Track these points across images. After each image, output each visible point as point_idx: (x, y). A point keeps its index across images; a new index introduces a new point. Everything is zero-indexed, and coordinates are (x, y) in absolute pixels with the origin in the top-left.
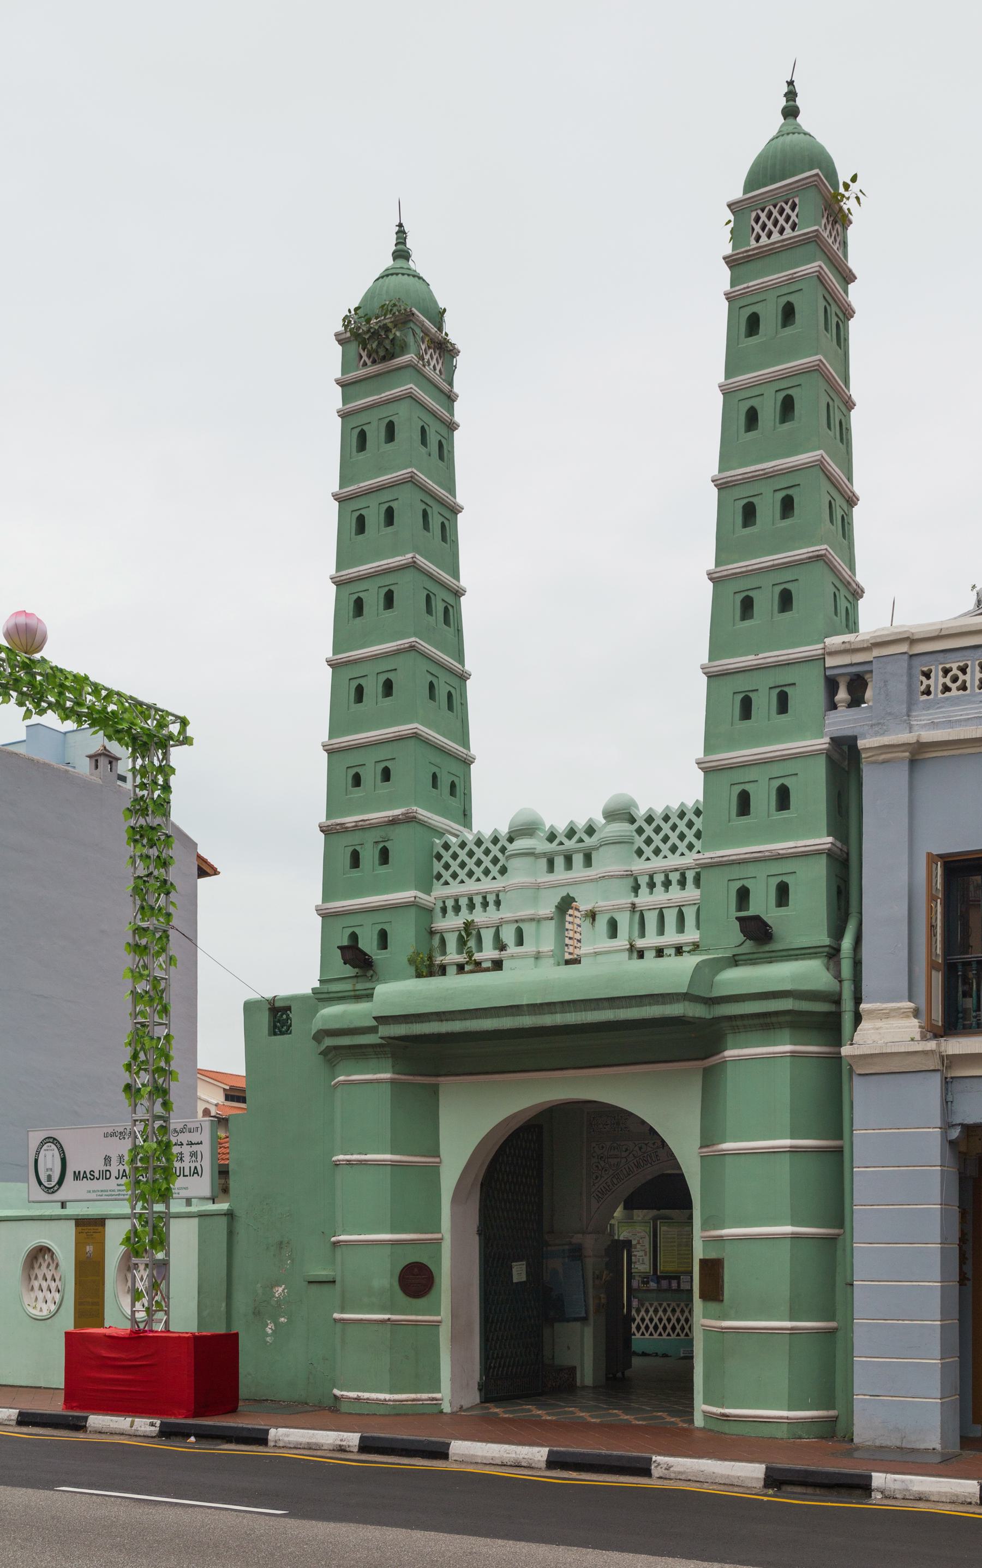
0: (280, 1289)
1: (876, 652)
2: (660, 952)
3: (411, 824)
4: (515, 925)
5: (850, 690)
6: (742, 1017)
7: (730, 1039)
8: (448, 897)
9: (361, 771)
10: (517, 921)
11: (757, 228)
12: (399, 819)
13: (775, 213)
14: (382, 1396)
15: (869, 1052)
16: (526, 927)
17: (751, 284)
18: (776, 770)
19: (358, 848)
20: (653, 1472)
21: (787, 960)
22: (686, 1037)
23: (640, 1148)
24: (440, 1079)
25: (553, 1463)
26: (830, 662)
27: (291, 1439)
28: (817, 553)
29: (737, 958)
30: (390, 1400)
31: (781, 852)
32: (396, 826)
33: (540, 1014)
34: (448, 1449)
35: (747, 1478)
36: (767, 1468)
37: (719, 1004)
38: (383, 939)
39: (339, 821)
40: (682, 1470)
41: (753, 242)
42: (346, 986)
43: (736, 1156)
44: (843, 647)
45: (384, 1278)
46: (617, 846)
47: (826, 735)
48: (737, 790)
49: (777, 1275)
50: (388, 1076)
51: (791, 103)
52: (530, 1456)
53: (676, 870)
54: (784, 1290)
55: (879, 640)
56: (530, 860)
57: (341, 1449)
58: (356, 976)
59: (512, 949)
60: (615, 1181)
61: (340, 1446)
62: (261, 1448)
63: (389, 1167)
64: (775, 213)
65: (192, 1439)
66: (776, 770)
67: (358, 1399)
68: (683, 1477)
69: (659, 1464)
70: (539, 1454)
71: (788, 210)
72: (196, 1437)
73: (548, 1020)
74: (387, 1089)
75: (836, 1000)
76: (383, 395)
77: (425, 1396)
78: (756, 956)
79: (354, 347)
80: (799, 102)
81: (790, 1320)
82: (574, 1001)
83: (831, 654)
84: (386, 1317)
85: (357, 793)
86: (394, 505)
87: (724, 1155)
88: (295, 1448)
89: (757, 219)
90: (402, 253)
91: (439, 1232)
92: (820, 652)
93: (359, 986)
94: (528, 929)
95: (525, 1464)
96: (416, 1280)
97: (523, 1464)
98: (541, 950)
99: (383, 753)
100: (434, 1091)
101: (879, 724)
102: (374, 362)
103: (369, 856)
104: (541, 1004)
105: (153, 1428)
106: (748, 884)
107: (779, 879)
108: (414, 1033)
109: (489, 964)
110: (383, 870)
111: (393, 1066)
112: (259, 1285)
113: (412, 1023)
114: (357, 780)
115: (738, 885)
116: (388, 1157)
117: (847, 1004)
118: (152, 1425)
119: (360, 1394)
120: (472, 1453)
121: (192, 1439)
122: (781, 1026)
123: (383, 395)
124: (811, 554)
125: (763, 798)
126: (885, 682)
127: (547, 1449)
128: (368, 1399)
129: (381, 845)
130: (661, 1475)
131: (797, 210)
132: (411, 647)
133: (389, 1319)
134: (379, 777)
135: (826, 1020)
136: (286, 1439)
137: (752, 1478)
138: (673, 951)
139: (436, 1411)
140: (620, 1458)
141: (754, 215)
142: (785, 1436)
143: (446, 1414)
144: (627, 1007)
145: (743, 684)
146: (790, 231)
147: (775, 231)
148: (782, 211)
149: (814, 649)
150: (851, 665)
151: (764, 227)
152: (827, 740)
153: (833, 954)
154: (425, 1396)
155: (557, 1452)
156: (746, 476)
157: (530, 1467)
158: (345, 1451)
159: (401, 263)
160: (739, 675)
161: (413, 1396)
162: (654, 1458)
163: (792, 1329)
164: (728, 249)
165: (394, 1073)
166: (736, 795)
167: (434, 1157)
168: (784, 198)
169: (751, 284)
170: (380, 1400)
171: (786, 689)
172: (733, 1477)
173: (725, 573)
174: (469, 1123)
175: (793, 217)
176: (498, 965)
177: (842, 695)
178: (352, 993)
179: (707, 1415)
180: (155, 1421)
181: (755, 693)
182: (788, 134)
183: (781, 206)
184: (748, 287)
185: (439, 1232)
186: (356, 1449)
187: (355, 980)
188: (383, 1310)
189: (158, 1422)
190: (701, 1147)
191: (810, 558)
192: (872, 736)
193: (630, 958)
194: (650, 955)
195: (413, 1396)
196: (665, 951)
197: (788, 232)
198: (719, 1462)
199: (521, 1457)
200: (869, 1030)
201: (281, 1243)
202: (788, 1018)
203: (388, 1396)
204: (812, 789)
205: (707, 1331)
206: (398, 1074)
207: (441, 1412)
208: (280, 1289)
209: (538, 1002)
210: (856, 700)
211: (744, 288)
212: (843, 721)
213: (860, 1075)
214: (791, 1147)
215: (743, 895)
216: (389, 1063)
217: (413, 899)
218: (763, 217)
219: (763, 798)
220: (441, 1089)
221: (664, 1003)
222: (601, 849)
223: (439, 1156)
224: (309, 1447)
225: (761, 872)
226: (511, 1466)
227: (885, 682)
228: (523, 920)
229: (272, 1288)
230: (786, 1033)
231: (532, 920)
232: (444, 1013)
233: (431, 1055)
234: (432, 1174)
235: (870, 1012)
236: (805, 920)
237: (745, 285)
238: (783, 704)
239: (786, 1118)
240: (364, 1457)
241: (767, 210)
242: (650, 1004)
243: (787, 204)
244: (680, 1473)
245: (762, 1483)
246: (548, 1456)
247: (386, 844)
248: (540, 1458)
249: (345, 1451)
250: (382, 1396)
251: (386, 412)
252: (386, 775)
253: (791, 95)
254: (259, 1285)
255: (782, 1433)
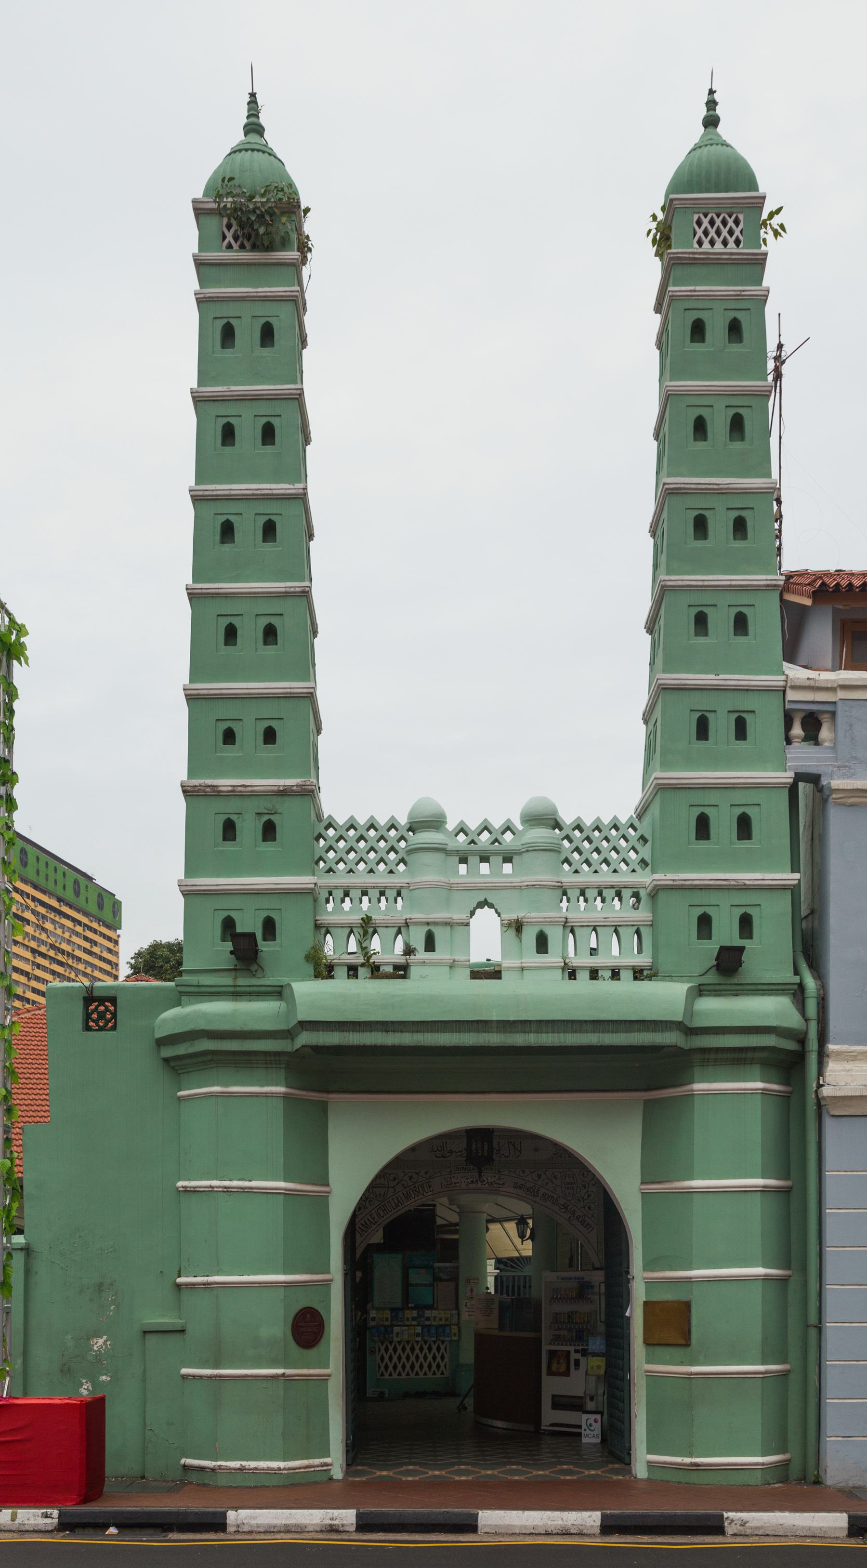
0: (101, 1341)
1: (841, 694)
2: (594, 974)
3: (306, 798)
4: (426, 928)
5: (804, 726)
6: (717, 1050)
7: (697, 1071)
8: (336, 888)
9: (236, 727)
10: (428, 924)
11: (700, 232)
12: (293, 791)
13: (718, 222)
14: (274, 1464)
15: (849, 1094)
16: (438, 932)
17: (698, 288)
18: (739, 797)
19: (234, 818)
20: (726, 1529)
21: (754, 995)
22: (642, 1069)
23: (411, 1178)
24: (331, 1096)
25: (607, 1528)
26: (791, 695)
27: (260, 1521)
28: (774, 583)
29: (702, 988)
30: (285, 1469)
31: (747, 883)
32: (285, 798)
33: (511, 1032)
34: (477, 1520)
35: (830, 1528)
36: (849, 1517)
37: (697, 1034)
38: (269, 927)
39: (209, 782)
40: (759, 1525)
41: (696, 246)
42: (226, 980)
43: (743, 1194)
44: (808, 683)
45: (276, 1327)
46: (548, 853)
47: (790, 769)
48: (697, 812)
49: (752, 1317)
50: (281, 1089)
51: (711, 112)
52: (579, 1522)
53: (612, 887)
54: (755, 1332)
55: (847, 683)
56: (439, 856)
57: (332, 1529)
58: (235, 970)
59: (421, 955)
60: (382, 1213)
61: (331, 1525)
62: (221, 1536)
63: (282, 1197)
64: (718, 222)
65: (113, 1530)
66: (739, 797)
67: (241, 1469)
68: (760, 1532)
69: (732, 1521)
70: (591, 1519)
71: (731, 223)
72: (117, 1526)
73: (519, 1039)
74: (280, 1104)
75: (802, 1040)
76: (260, 290)
77: (317, 1461)
78: (721, 987)
79: (215, 224)
80: (719, 111)
81: (762, 1364)
82: (553, 1022)
83: (793, 687)
84: (280, 1371)
85: (231, 752)
86: (275, 422)
87: (691, 1192)
88: (266, 1532)
89: (699, 223)
90: (254, 128)
91: (329, 1272)
92: (782, 684)
93: (241, 982)
94: (440, 934)
95: (575, 1532)
96: (307, 1328)
97: (572, 1531)
98: (457, 958)
99: (268, 710)
100: (323, 1108)
101: (845, 766)
102: (242, 247)
103: (249, 828)
104: (515, 1022)
105: (48, 1521)
106: (710, 911)
107: (742, 910)
108: (351, 1043)
109: (390, 969)
110: (268, 847)
111: (286, 1079)
112: (69, 1337)
113: (348, 1031)
114: (229, 737)
115: (699, 911)
116: (282, 1184)
117: (813, 1044)
118: (46, 1516)
119: (244, 1463)
120: (507, 1523)
121: (113, 1530)
122: (752, 1062)
123: (260, 290)
124: (769, 582)
125: (723, 825)
126: (851, 725)
127: (599, 1513)
128: (256, 1469)
129: (265, 818)
130: (735, 1531)
131: (741, 226)
132: (303, 592)
133: (283, 1375)
134: (261, 738)
135: (791, 1061)
136: (253, 1522)
137: (836, 1528)
138: (609, 974)
139: (325, 1478)
140: (686, 1517)
141: (696, 217)
142: (759, 1483)
143: (338, 1481)
144: (613, 1032)
145: (703, 703)
146: (734, 246)
147: (706, 242)
148: (724, 223)
149: (775, 680)
150: (813, 702)
151: (706, 233)
152: (792, 775)
153: (798, 993)
154: (317, 1461)
155: (612, 1516)
156: (700, 486)
157: (581, 1534)
158: (337, 1531)
159: (254, 138)
160: (697, 692)
161: (305, 1462)
162: (726, 1515)
163: (766, 1372)
164: (199, 195)
165: (287, 1087)
166: (684, 816)
167: (323, 1185)
168: (729, 210)
169: (698, 288)
170: (273, 1469)
171: (744, 715)
172: (816, 1528)
173: (680, 583)
174: (359, 1152)
175: (737, 232)
176: (401, 971)
177: (797, 730)
178: (231, 989)
179: (650, 1465)
180: (49, 1511)
181: (750, 715)
182: (706, 145)
183: (724, 217)
184: (695, 291)
185: (329, 1272)
186: (353, 1528)
187: (233, 973)
188: (273, 1364)
189: (55, 1513)
190: (642, 1183)
191: (768, 586)
192: (839, 778)
193: (563, 978)
194: (583, 976)
195: (305, 1462)
196: (600, 973)
197: (719, 247)
198: (797, 1514)
199: (570, 1523)
200: (839, 1071)
201: (101, 1285)
202: (765, 1054)
203: (282, 1464)
204: (771, 820)
205: (651, 1377)
206: (292, 1088)
207: (331, 1479)
208: (101, 1341)
209: (512, 1019)
210: (812, 735)
211: (691, 291)
212: (802, 756)
213: (833, 1116)
214: (763, 1187)
215: (705, 923)
216: (282, 1074)
217: (312, 886)
218: (706, 222)
219: (723, 825)
220: (330, 1108)
221: (655, 1031)
222: (524, 854)
223: (328, 1185)
224: (287, 1529)
225: (724, 901)
226: (557, 1534)
227: (851, 725)
228: (436, 924)
229: (88, 1339)
230: (756, 1070)
231: (447, 924)
232: (393, 1023)
233: (333, 1069)
234: (321, 1203)
235: (838, 1054)
236: (770, 952)
237: (692, 288)
238: (741, 730)
239: (757, 1158)
240: (615, 1541)
241: (709, 217)
242: (639, 1031)
243: (730, 217)
244: (757, 1528)
245: (846, 1532)
246: (602, 1520)
247: (273, 818)
248: (592, 1523)
249: (337, 1531)
250: (274, 1464)
251: (267, 311)
252: (270, 736)
253: (711, 104)
254: (69, 1337)
255: (755, 1479)
